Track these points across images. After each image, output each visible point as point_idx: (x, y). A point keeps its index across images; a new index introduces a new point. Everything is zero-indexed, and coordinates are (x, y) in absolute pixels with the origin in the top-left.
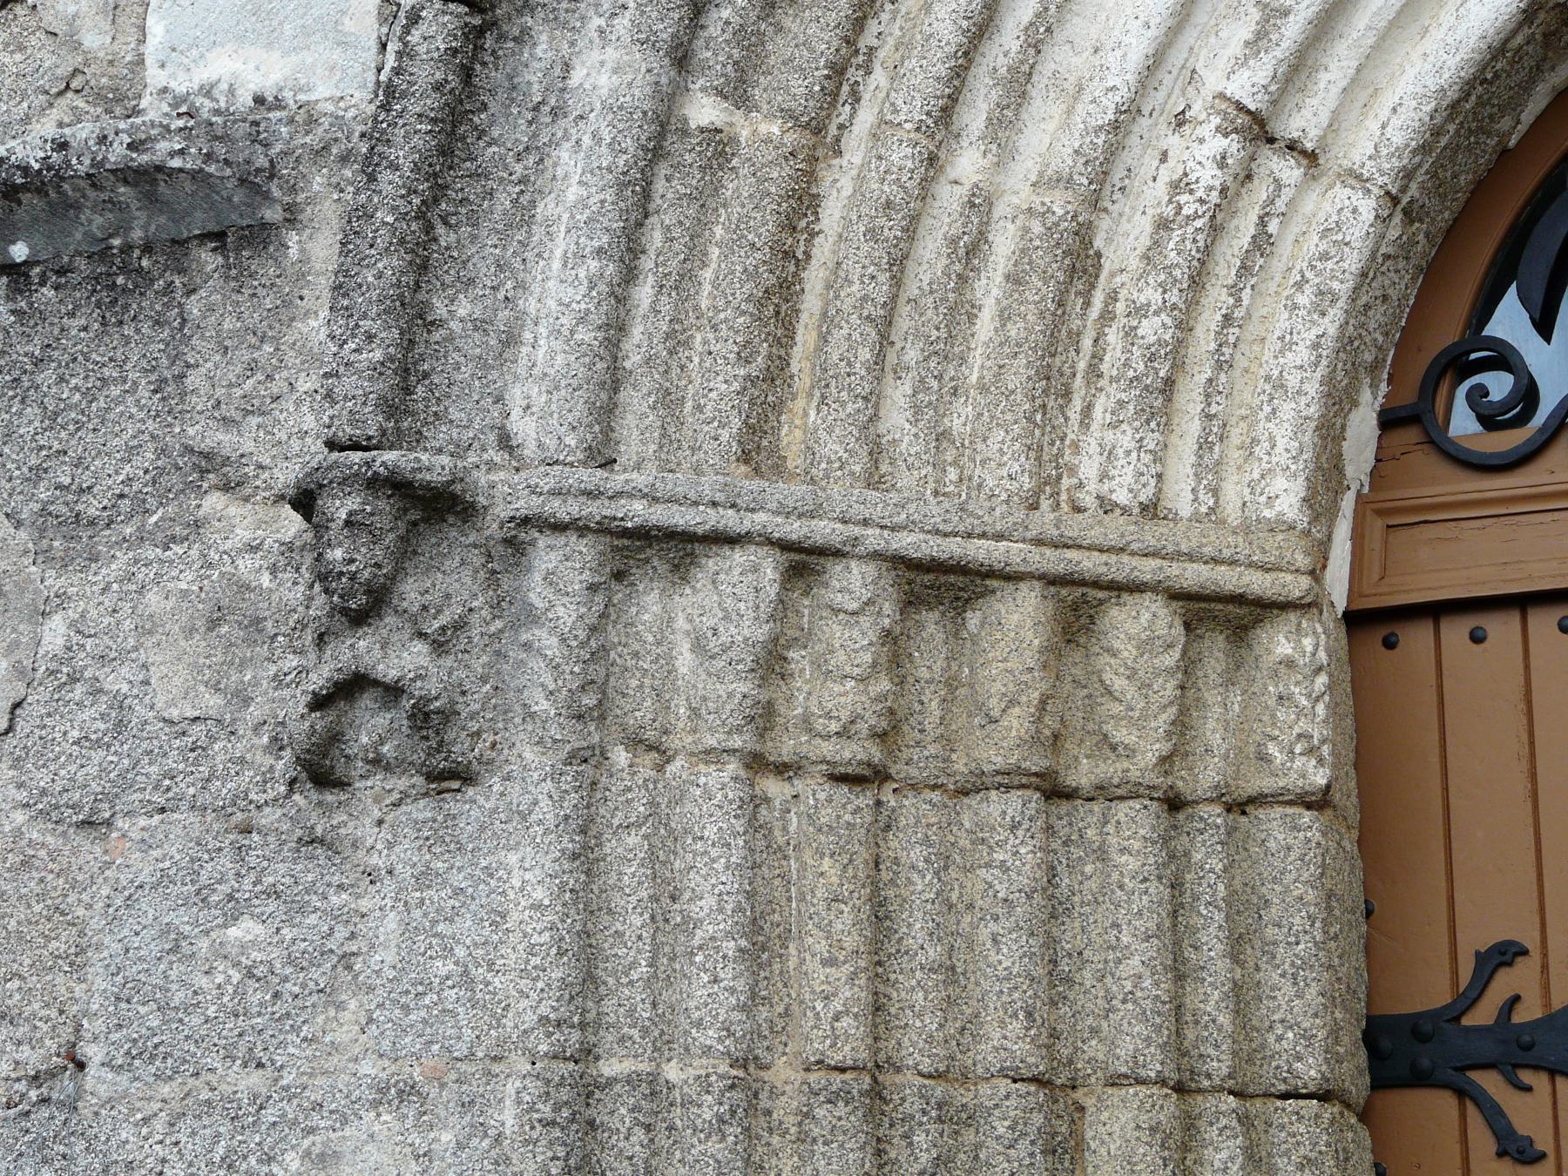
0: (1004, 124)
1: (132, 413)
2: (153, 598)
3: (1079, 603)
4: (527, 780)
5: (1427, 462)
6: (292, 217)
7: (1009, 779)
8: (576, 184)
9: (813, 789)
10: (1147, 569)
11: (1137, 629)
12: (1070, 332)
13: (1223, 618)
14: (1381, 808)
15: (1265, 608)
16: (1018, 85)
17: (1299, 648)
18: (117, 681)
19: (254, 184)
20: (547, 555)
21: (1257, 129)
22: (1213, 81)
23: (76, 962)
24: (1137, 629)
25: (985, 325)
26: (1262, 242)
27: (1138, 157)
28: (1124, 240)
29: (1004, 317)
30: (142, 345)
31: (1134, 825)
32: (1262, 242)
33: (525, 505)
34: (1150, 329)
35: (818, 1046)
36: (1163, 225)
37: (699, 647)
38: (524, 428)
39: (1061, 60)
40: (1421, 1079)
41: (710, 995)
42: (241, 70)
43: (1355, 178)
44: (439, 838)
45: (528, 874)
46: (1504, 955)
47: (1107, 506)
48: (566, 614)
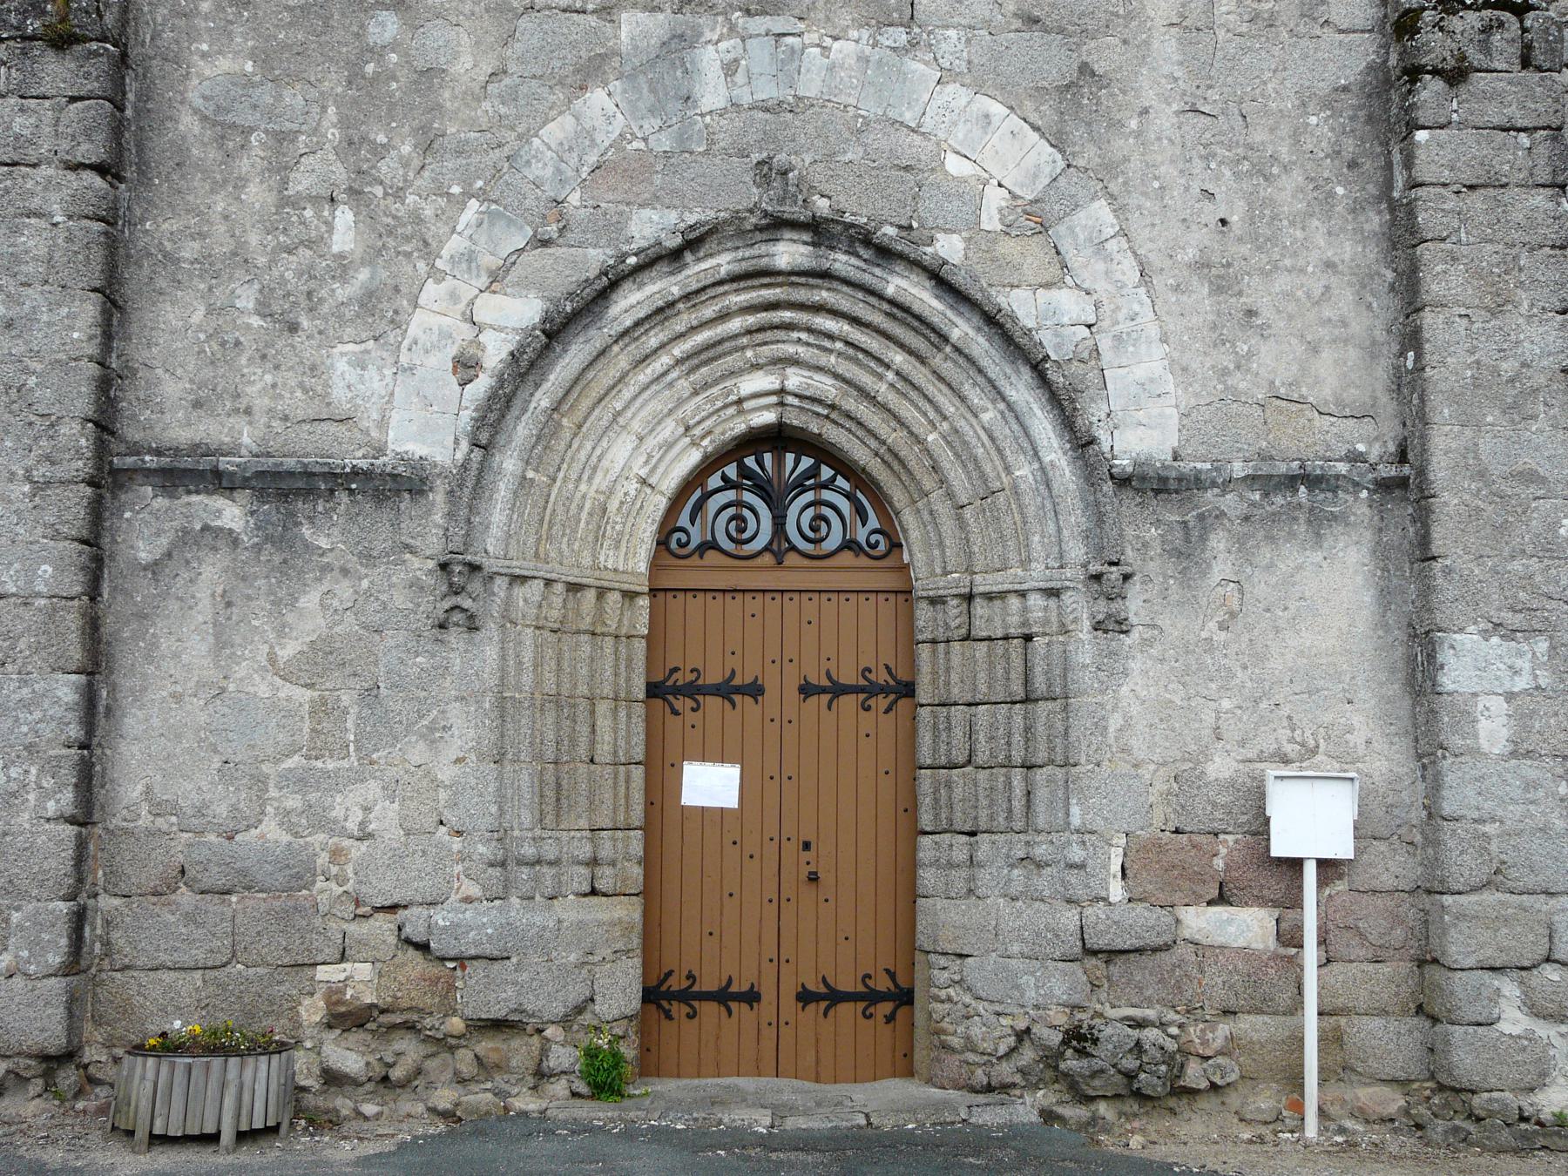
0: (590, 479)
1: (385, 530)
2: (394, 579)
3: (602, 592)
4: (491, 630)
5: (665, 554)
6: (431, 489)
7: (585, 632)
8: (503, 490)
9: (546, 633)
10: (617, 585)
11: (614, 598)
12: (60, 22)
13: (630, 595)
14: (655, 640)
15: (637, 594)
16: (595, 469)
17: (644, 602)
18: (384, 597)
19: (423, 481)
20: (498, 581)
21: (644, 482)
22: (635, 470)
23: (376, 663)
24: (614, 598)
25: (582, 524)
26: (641, 507)
27: (619, 487)
28: (613, 505)
29: (588, 523)
30: (386, 514)
31: (609, 641)
32: (641, 507)
33: (495, 569)
34: (618, 527)
35: (546, 690)
36: (622, 503)
37: (525, 600)
38: (490, 549)
39: (605, 463)
40: (656, 696)
41: (527, 679)
42: (417, 449)
43: (662, 493)
44: (470, 642)
45: (491, 652)
46: (676, 670)
47: (606, 568)
48: (502, 594)
